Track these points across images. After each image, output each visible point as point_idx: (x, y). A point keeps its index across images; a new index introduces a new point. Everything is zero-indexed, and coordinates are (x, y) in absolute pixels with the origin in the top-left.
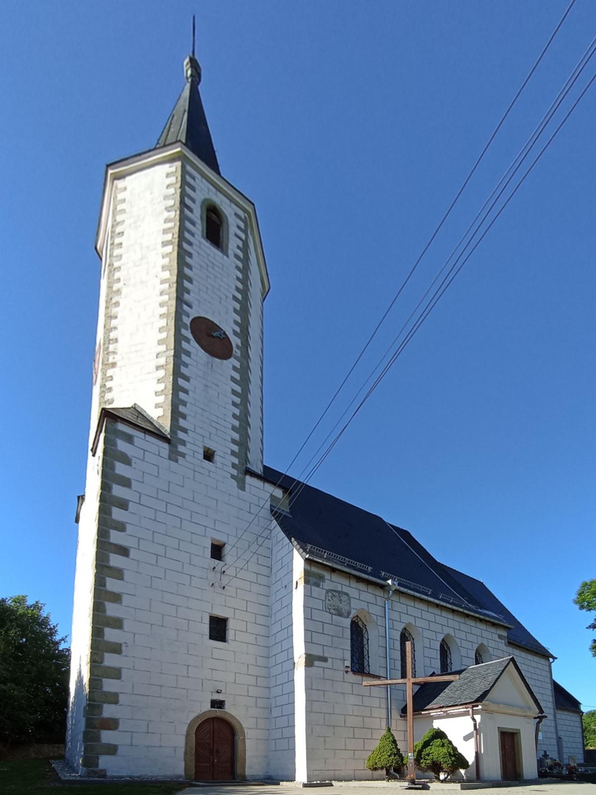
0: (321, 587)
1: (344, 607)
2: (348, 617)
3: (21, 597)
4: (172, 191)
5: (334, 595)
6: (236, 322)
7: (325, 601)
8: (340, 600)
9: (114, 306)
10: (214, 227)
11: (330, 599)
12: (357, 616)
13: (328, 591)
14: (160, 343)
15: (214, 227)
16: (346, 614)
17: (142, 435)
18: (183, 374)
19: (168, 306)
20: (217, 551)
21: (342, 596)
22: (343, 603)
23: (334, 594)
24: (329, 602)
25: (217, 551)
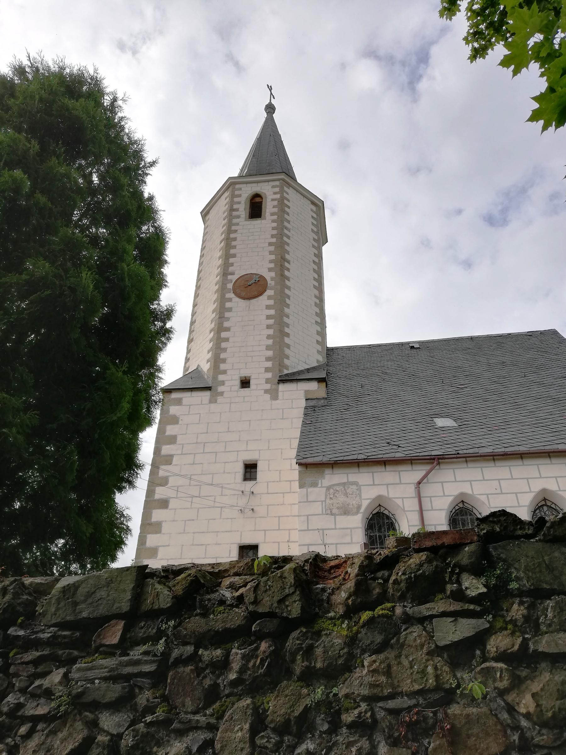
0: (320, 485)
1: (353, 502)
2: (357, 513)
3: (209, 577)
4: (226, 214)
5: (337, 491)
6: (288, 270)
7: (325, 501)
8: (346, 495)
9: (422, 66)
10: (256, 209)
11: (332, 496)
12: (380, 505)
13: (328, 488)
14: (258, 200)
15: (256, 209)
16: (355, 510)
17: (245, 185)
18: (224, 338)
19: (258, 558)
20: (250, 470)
21: (348, 488)
22: (351, 496)
23: (338, 489)
24: (331, 502)
25: (250, 470)
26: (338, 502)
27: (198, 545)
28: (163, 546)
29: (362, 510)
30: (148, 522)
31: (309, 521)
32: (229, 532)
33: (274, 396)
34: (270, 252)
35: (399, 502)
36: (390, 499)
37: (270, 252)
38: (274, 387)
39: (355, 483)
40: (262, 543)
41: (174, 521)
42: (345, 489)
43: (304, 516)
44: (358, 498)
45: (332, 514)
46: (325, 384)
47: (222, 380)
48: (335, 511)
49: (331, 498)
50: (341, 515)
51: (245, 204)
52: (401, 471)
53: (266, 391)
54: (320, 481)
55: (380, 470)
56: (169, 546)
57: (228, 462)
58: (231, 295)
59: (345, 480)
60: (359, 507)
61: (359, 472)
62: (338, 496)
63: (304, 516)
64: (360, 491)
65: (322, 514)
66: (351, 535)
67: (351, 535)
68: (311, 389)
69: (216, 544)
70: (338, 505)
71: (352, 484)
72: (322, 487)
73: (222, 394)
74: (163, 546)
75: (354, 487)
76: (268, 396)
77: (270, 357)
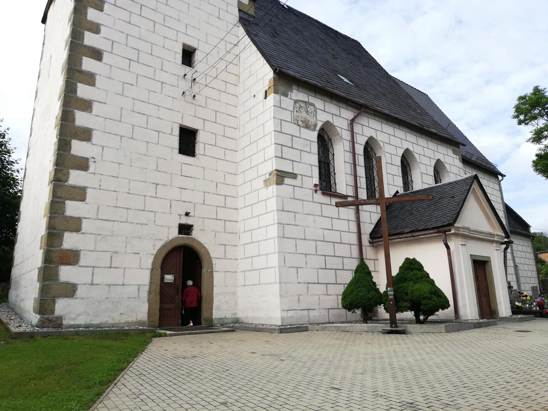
1: (312, 120)
2: (314, 130)
8: (307, 112)
18: (92, 23)
20: (188, 56)
24: (297, 114)
25: (188, 56)
28: (99, 102)
29: (318, 128)
30: (78, 68)
34: (83, 199)
36: (334, 126)
37: (83, 199)
39: (313, 105)
44: (315, 118)
46: (95, 103)
47: (75, 214)
48: (300, 123)
49: (297, 111)
50: (304, 127)
60: (315, 126)
61: (315, 97)
64: (316, 113)
65: (291, 122)
71: (311, 105)
74: (99, 102)
75: (312, 108)
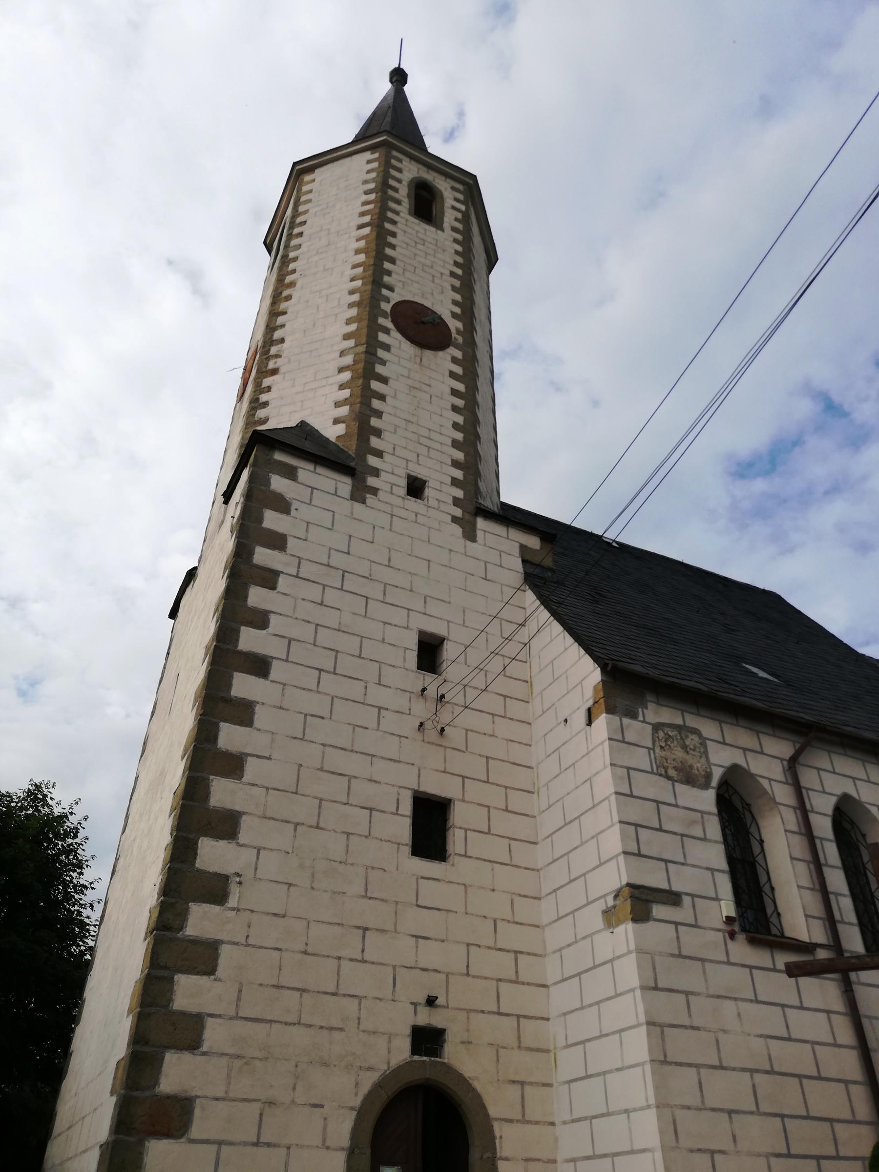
7: (653, 749)
8: (685, 747)
11: (663, 744)
13: (657, 727)
17: (408, 159)
20: (429, 653)
24: (663, 754)
25: (429, 653)
26: (674, 757)
27: (333, 773)
29: (715, 782)
31: (632, 781)
32: (395, 761)
33: (470, 535)
35: (765, 783)
38: (467, 516)
39: (696, 731)
40: (459, 800)
41: (281, 708)
42: (681, 738)
43: (622, 767)
44: (703, 760)
45: (669, 778)
48: (672, 773)
49: (662, 747)
50: (682, 782)
51: (409, 190)
52: (762, 733)
53: (455, 519)
54: (640, 710)
55: (729, 720)
56: (269, 758)
57: (390, 624)
58: (388, 323)
59: (679, 721)
62: (672, 745)
63: (622, 767)
66: (703, 824)
67: (703, 824)
68: (530, 546)
69: (370, 780)
70: (676, 764)
72: (644, 721)
73: (374, 491)
76: (457, 530)
77: (460, 463)
